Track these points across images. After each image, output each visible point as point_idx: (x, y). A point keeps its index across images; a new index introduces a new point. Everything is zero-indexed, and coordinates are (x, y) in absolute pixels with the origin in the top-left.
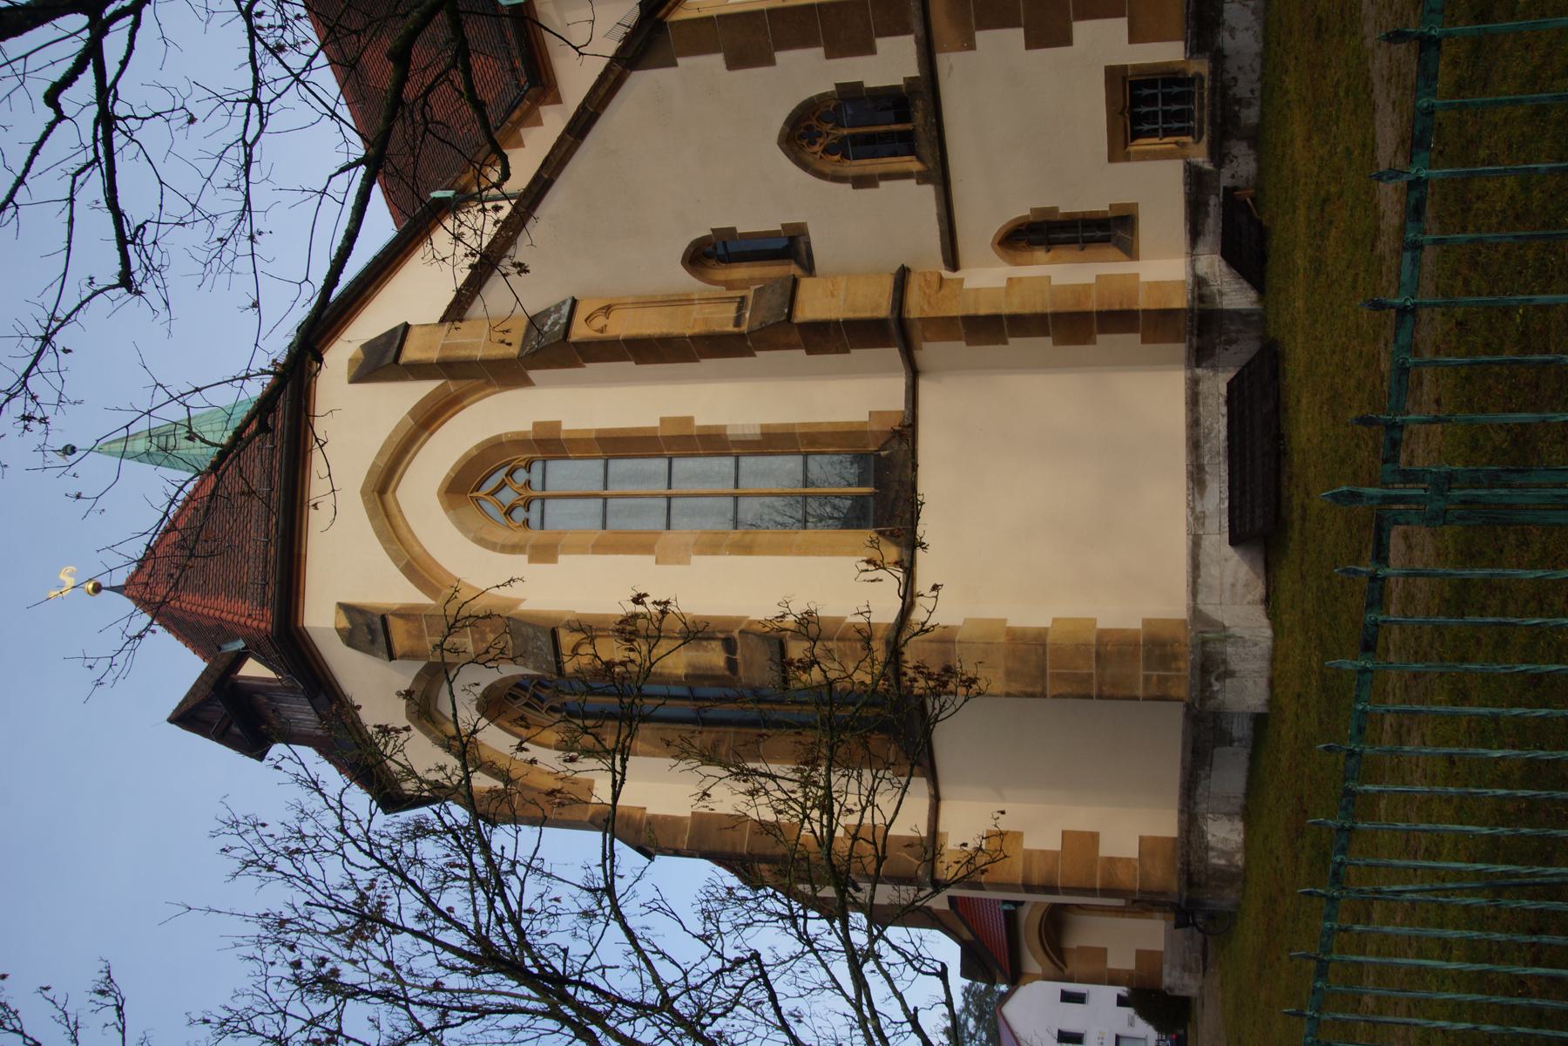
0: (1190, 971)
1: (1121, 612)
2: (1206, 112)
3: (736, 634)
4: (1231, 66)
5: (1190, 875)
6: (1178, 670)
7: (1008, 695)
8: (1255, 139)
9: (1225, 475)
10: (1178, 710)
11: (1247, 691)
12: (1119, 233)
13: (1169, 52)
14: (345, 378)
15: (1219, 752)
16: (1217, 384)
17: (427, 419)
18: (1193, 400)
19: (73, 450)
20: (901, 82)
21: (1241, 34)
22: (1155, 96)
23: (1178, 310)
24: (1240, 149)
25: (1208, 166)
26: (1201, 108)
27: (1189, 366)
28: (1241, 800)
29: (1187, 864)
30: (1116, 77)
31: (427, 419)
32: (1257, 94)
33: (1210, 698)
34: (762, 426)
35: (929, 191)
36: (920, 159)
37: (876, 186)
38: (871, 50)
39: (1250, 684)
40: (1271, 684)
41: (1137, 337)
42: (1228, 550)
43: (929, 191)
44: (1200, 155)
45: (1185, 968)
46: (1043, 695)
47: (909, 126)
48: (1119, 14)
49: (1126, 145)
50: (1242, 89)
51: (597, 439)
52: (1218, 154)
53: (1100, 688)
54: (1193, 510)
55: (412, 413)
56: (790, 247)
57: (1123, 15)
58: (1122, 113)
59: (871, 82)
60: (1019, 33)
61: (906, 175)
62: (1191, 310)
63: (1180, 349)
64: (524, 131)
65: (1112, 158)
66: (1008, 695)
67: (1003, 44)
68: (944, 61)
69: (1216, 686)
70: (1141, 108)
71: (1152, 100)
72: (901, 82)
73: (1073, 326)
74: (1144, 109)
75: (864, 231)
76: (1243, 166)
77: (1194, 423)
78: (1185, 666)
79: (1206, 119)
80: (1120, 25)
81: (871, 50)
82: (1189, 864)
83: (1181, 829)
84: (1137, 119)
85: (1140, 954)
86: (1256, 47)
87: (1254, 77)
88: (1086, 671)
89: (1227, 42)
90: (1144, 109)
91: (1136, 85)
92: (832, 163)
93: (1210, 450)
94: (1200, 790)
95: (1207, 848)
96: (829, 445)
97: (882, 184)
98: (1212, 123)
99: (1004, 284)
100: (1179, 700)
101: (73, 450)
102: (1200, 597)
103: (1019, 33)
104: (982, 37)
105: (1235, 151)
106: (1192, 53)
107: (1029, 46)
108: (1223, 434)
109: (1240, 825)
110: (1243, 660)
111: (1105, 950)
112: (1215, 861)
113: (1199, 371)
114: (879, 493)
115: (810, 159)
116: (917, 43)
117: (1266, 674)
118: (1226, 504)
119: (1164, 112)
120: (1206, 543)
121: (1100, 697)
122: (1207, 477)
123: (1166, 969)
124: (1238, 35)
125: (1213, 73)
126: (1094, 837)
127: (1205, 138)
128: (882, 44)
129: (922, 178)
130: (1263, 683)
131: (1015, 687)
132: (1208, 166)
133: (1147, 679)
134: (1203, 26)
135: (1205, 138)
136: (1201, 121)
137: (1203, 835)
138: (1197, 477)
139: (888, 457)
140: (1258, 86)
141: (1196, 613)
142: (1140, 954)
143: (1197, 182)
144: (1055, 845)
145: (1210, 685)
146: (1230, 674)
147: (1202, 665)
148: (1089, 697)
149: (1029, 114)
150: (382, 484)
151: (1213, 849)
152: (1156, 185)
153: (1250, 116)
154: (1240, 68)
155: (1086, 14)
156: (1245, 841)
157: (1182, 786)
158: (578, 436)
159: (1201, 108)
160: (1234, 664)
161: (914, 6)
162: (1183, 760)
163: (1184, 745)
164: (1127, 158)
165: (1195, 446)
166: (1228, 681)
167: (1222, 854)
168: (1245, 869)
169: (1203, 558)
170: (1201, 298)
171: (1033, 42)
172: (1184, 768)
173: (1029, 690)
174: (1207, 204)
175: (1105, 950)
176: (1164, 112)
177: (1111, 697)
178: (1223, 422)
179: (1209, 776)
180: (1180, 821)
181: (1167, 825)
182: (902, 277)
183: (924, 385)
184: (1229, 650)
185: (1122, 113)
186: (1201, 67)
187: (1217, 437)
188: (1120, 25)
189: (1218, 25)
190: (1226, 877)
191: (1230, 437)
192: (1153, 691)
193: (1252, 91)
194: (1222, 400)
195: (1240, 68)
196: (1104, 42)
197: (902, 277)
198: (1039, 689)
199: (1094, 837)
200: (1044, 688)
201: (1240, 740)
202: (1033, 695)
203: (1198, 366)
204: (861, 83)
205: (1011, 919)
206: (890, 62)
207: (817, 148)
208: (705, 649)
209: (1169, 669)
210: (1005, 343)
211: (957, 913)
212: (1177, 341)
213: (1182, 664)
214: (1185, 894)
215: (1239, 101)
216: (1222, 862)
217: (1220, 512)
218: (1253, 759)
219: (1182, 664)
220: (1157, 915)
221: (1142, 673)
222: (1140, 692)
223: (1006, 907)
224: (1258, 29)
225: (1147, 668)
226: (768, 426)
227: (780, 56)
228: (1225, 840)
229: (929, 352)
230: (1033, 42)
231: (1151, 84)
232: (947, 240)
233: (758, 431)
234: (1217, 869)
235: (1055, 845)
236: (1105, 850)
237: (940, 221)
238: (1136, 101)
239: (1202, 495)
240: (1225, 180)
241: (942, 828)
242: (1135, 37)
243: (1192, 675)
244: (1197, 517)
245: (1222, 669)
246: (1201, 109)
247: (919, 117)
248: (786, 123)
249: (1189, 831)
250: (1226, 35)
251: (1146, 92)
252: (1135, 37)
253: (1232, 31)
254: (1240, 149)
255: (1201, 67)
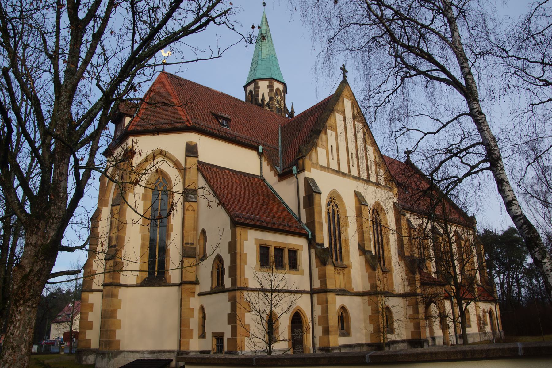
1: (120, 335)
9: (152, 359)
14: (187, 141)
17: (176, 164)
18: (170, 352)
19: (264, 6)
29: (84, 351)
31: (176, 164)
35: (209, 290)
55: (177, 160)
64: (273, 171)
65: (212, 333)
68: (227, 294)
73: (183, 323)
77: (164, 352)
95: (87, 355)
99: (191, 307)
101: (264, 6)
102: (126, 353)
108: (161, 358)
114: (155, 275)
126: (91, 329)
137: (91, 354)
138: (152, 352)
141: (122, 352)
144: (90, 320)
150: (162, 153)
152: (208, 344)
165: (159, 352)
167: (86, 359)
169: (134, 353)
183: (177, 287)
184: (106, 359)
191: (161, 360)
199: (91, 329)
227: (230, 254)
235: (90, 320)
236: (88, 332)
241: (94, 293)
244: (143, 352)
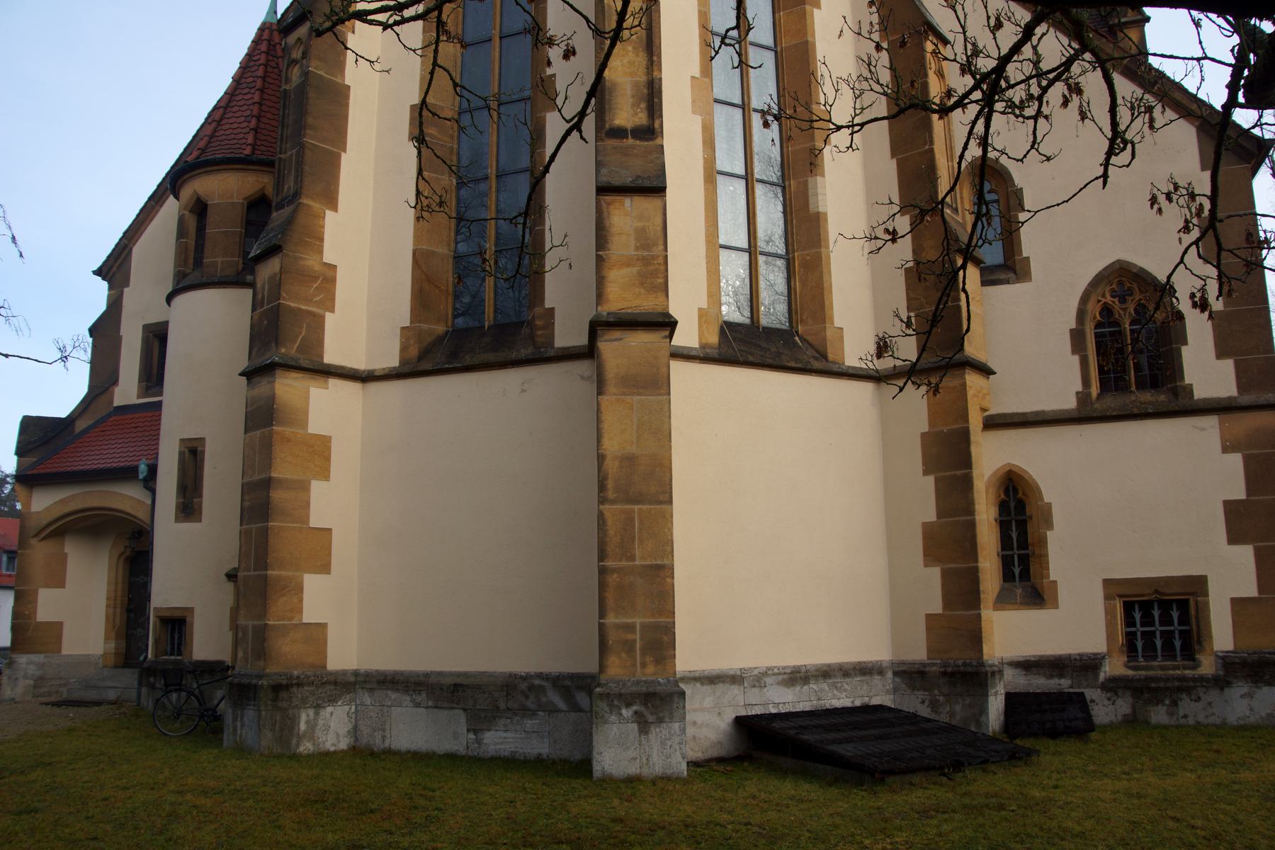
0: (35, 687)
2: (1160, 673)
3: (658, 141)
4: (1213, 695)
5: (287, 687)
6: (644, 665)
7: (601, 458)
8: (1132, 721)
9: (801, 707)
10: (591, 667)
11: (619, 750)
12: (1019, 591)
13: (1222, 635)
15: (461, 717)
16: (880, 694)
18: (865, 670)
20: (1187, 381)
21: (1242, 704)
22: (1171, 623)
23: (981, 650)
24: (1123, 706)
25: (1102, 676)
26: (1162, 668)
27: (892, 663)
28: (378, 743)
30: (1198, 585)
32: (1182, 721)
33: (611, 706)
34: (826, 214)
35: (1069, 403)
36: (1099, 396)
37: (1074, 352)
38: (1221, 354)
39: (631, 753)
40: (632, 781)
41: (937, 607)
42: (730, 715)
43: (1070, 403)
44: (1115, 667)
45: (40, 681)
46: (602, 500)
47: (1133, 388)
48: (1261, 589)
49: (1120, 596)
50: (1187, 706)
51: (806, 42)
52: (1114, 686)
53: (614, 570)
54: (765, 674)
56: (1011, 268)
57: (1260, 591)
58: (1157, 592)
59: (1188, 354)
60: (1241, 494)
61: (1086, 381)
62: (982, 664)
63: (918, 652)
65: (1107, 583)
66: (601, 458)
67: (1229, 477)
68: (1210, 423)
69: (626, 713)
70: (1158, 614)
71: (1166, 620)
72: (1187, 381)
74: (1156, 613)
75: (1027, 336)
76: (1104, 711)
78: (649, 672)
79: (1151, 673)
80: (1249, 589)
81: (1221, 354)
82: (299, 685)
83: (336, 673)
84: (1146, 606)
85: (57, 627)
86: (1232, 719)
87: (1201, 718)
88: (638, 553)
89: (1239, 690)
90: (1156, 613)
91: (1183, 605)
92: (1094, 309)
93: (822, 690)
94: (394, 696)
95: (318, 707)
96: (803, 283)
97: (1076, 358)
98: (1147, 679)
100: (602, 667)
103: (1241, 494)
104: (1236, 460)
105: (1120, 702)
106: (1223, 658)
107: (1227, 504)
109: (343, 745)
110: (663, 743)
111: (63, 587)
112: (304, 718)
113: (890, 675)
115: (1100, 291)
116: (1229, 398)
117: (645, 772)
118: (774, 711)
119: (1153, 633)
120: (735, 690)
121: (603, 571)
122: (798, 688)
123: (39, 658)
124: (1245, 702)
125: (1202, 679)
127: (1130, 673)
128: (1228, 365)
129: (1083, 398)
130: (633, 770)
131: (611, 466)
132: (1102, 676)
133: (630, 628)
134: (1251, 668)
135: (1130, 673)
136: (1150, 668)
137: (332, 700)
138: (797, 677)
139: (795, 343)
140: (1191, 721)
142: (57, 627)
143: (1087, 665)
145: (628, 705)
146: (644, 726)
147: (654, 694)
148: (602, 555)
149: (1136, 503)
151: (317, 714)
153: (1159, 715)
154: (1210, 704)
155: (1261, 560)
156: (327, 754)
157: (396, 673)
158: (808, 22)
159: (1162, 668)
160: (657, 733)
161: (1270, 397)
162: (440, 674)
163: (466, 675)
164: (1107, 597)
166: (635, 726)
167: (312, 726)
168: (296, 757)
169: (720, 688)
170: (993, 673)
171: (1231, 508)
172: (427, 675)
173: (610, 484)
174: (1061, 676)
175: (63, 587)
176: (1153, 633)
177: (602, 586)
178: (847, 703)
179: (418, 705)
180: (344, 672)
181: (342, 656)
182: (986, 371)
183: (867, 388)
185: (1157, 592)
186: (1207, 666)
187: (834, 697)
188: (1249, 589)
189: (1255, 682)
190: (286, 729)
192: (612, 637)
193: (1185, 716)
194: (866, 699)
195: (1210, 704)
196: (1232, 574)
197: (986, 371)
198: (611, 494)
199: (324, 567)
200: (613, 502)
201: (479, 741)
202: (602, 487)
203: (896, 674)
204: (1186, 343)
205: (126, 474)
206: (1206, 369)
207: (1109, 299)
208: (635, 105)
209: (643, 654)
210: (926, 473)
211: (109, 415)
212: (929, 651)
213: (651, 669)
214: (264, 682)
215: (1175, 704)
216: (303, 727)
217: (765, 705)
218: (452, 757)
219: (651, 669)
220: (112, 645)
221: (638, 621)
222: (611, 619)
223: (143, 468)
224: (1252, 719)
225: (643, 626)
226: (826, 220)
228: (327, 728)
229: (915, 400)
230: (1231, 508)
231: (1184, 620)
232: (1016, 420)
233: (821, 209)
234: (294, 721)
237: (1037, 413)
238: (1165, 605)
239: (781, 683)
240: (1090, 694)
241: (333, 383)
242: (1238, 604)
243: (638, 683)
244: (758, 679)
245: (651, 718)
246: (1158, 668)
247: (1147, 396)
248: (1142, 269)
249: (336, 683)
250: (1245, 690)
251: (1175, 615)
252: (1238, 604)
253: (1250, 695)
254: (1123, 706)
255: (1207, 666)
